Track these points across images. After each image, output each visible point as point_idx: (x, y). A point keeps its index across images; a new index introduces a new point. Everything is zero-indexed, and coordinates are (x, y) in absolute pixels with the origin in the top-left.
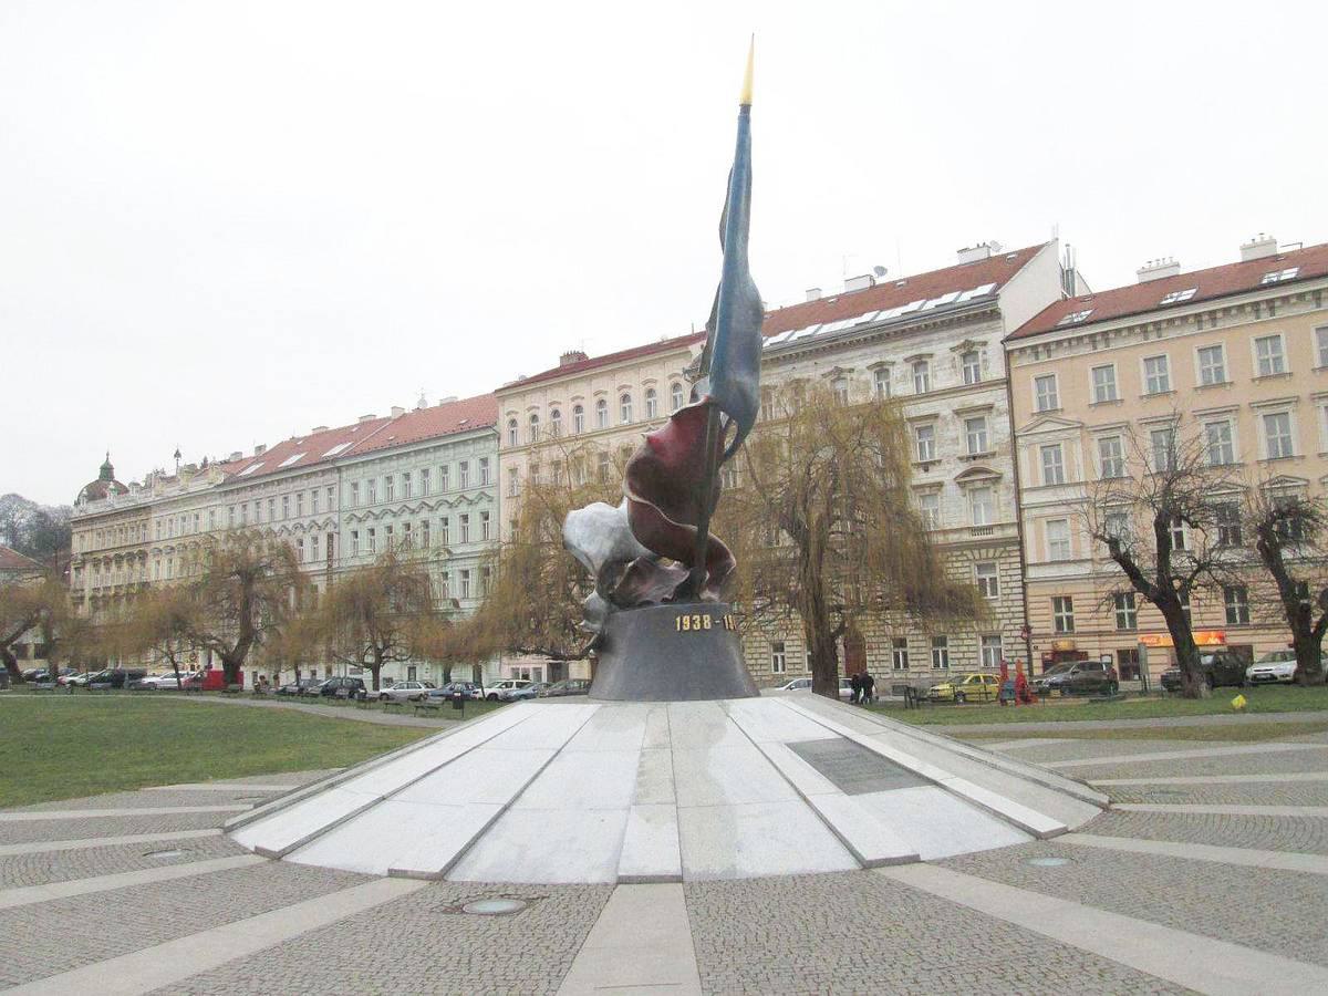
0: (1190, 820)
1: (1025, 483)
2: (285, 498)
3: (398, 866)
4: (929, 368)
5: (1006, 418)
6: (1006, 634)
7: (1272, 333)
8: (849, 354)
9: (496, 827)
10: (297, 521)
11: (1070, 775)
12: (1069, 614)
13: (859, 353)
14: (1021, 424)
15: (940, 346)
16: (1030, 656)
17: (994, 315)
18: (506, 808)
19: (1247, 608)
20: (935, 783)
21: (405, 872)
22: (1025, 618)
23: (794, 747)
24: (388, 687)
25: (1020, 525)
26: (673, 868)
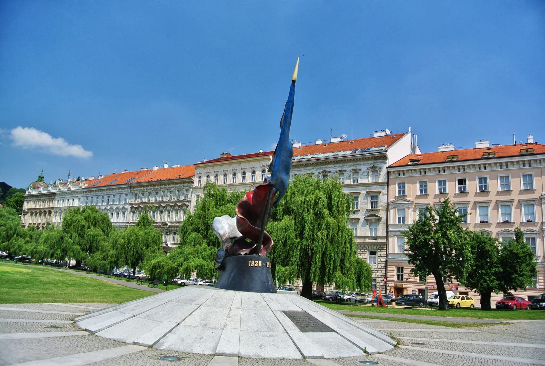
0: (423, 353)
1: (391, 222)
2: (120, 195)
4: (359, 175)
5: (386, 197)
6: (378, 279)
7: (506, 175)
8: (330, 166)
9: (174, 330)
11: (386, 334)
12: (402, 274)
13: (333, 166)
14: (391, 199)
15: (364, 167)
16: (386, 288)
17: (385, 158)
19: (403, 275)
20: (335, 331)
21: (139, 343)
22: (385, 273)
23: (286, 313)
24: (140, 274)
25: (387, 238)
26: (236, 352)
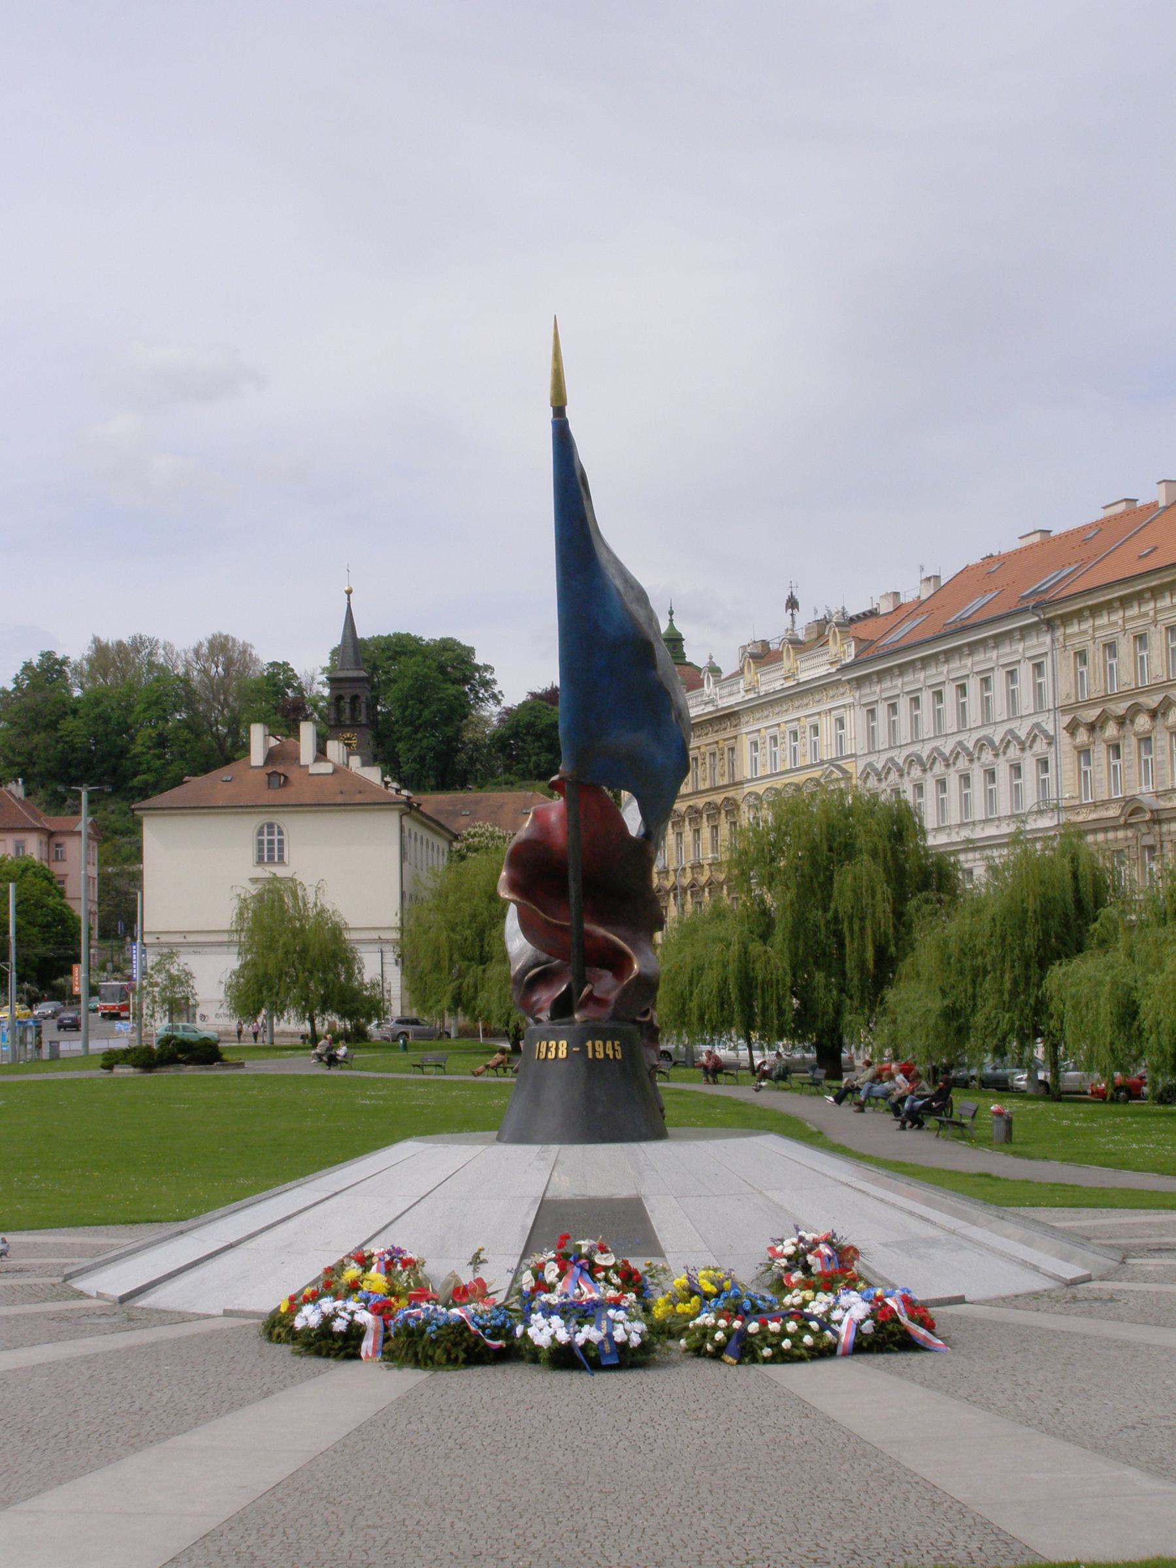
3: (229, 1307)
10: (1007, 726)
18: (231, 1246)
